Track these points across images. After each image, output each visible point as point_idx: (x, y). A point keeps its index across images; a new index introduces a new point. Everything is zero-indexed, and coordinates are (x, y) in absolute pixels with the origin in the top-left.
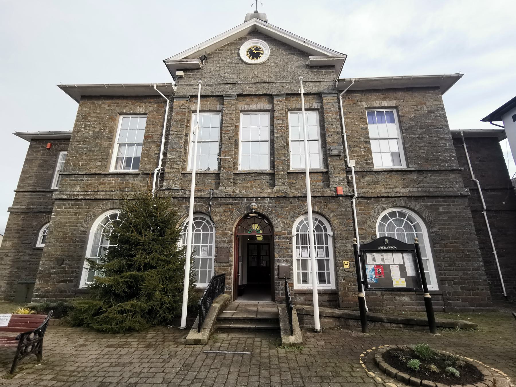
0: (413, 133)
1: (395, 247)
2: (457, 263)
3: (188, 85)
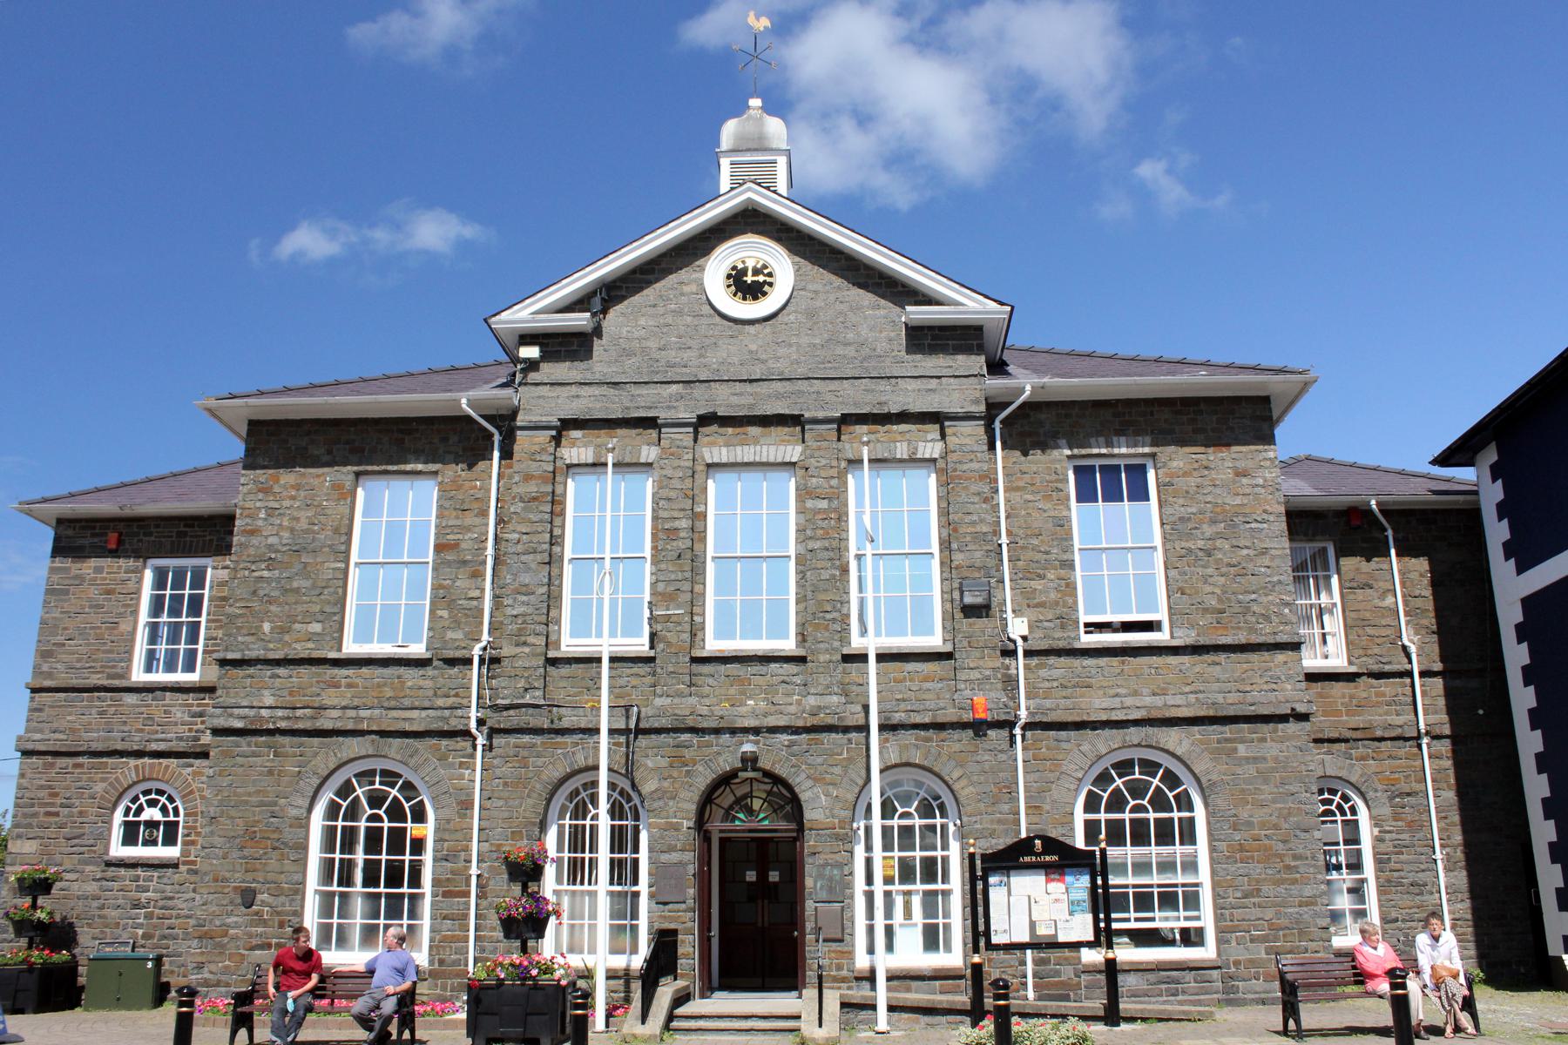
0: (1189, 536)
1: (1055, 858)
2: (1265, 889)
3: (552, 384)
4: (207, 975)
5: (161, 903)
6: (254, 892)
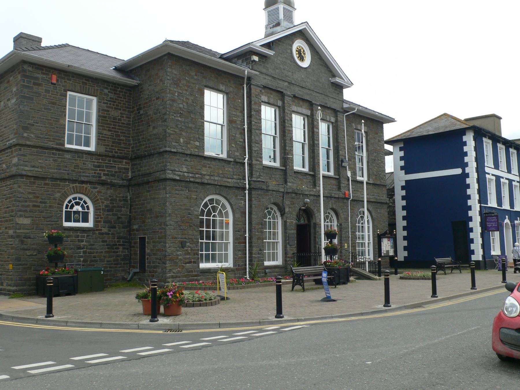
4: (172, 274)
5: (89, 247)
6: (186, 242)
